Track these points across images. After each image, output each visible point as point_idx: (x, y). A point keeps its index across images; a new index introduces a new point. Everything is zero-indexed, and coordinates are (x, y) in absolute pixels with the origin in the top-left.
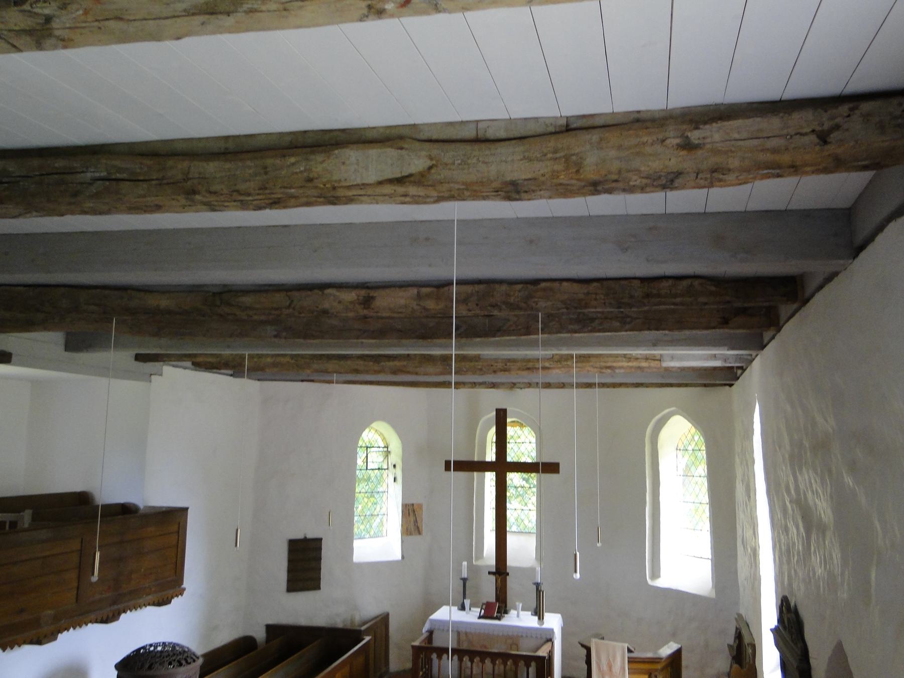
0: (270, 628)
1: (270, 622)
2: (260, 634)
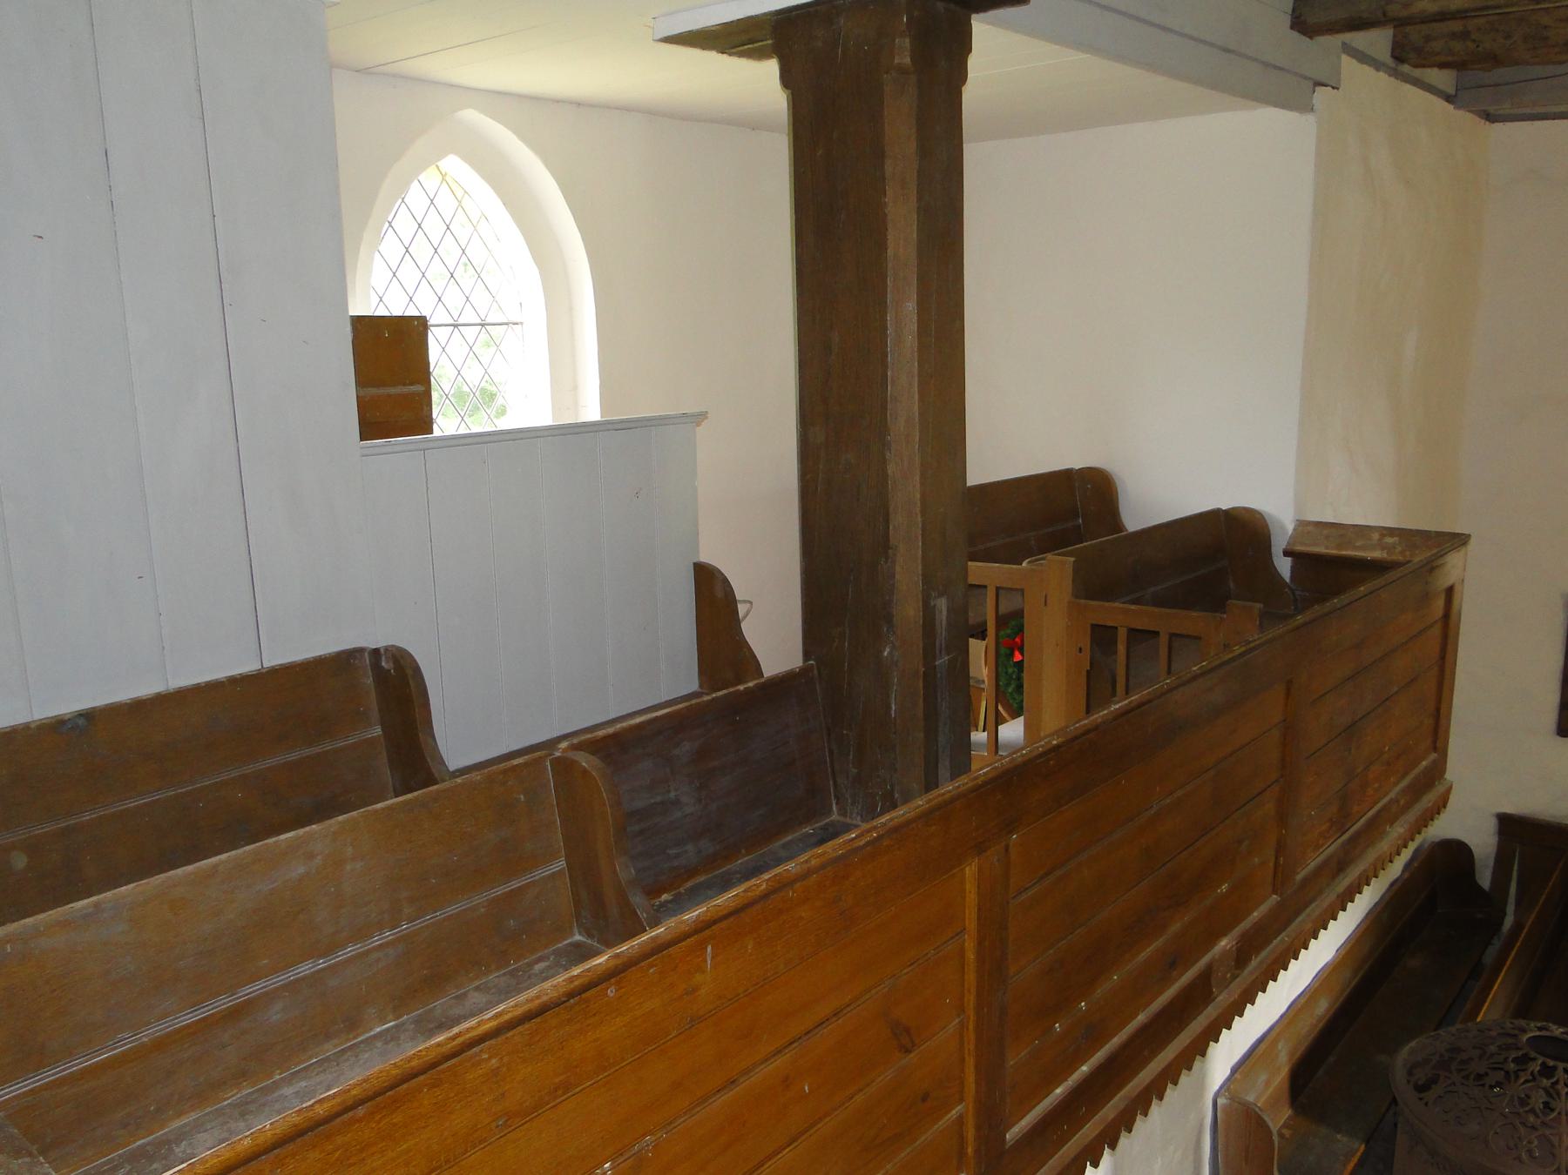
0: (1510, 826)
1: (1509, 809)
2: (1482, 840)
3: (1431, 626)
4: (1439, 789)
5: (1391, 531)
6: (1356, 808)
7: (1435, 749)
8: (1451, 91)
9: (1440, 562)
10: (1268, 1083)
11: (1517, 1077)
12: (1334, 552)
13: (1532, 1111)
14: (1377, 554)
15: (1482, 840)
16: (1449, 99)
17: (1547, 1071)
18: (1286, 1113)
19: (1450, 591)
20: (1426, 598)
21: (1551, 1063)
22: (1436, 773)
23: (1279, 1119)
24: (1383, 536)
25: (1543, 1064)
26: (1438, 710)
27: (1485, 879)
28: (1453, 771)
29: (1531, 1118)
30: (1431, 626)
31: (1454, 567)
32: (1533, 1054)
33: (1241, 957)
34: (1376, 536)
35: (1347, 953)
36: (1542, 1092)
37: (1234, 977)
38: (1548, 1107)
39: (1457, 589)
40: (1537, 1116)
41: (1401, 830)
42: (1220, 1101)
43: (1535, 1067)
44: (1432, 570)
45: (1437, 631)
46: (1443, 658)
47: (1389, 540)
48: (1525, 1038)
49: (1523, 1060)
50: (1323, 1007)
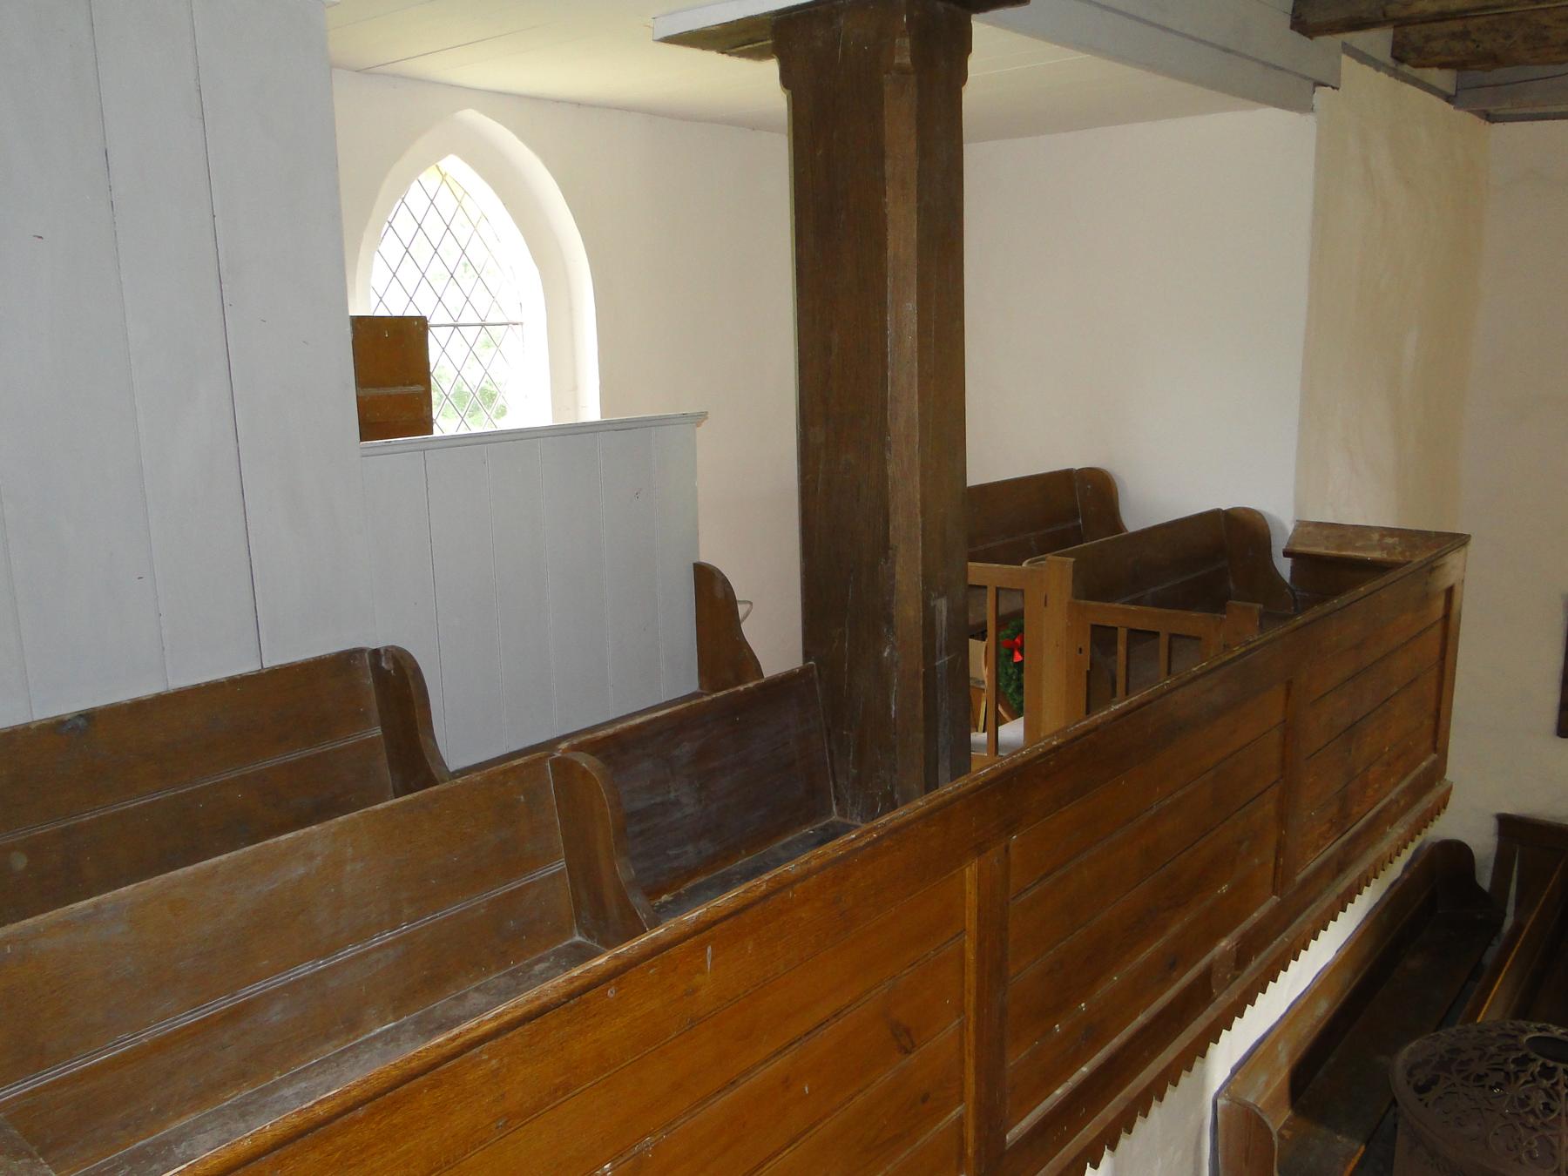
0: (1510, 827)
1: (1509, 809)
2: (1482, 841)
3: (1431, 626)
4: (1439, 790)
5: (1391, 532)
6: (1356, 809)
7: (1435, 750)
8: (1452, 91)
9: (1440, 562)
10: (1268, 1084)
11: (1517, 1078)
12: (1334, 552)
13: (1533, 1112)
14: (1377, 555)
15: (1482, 841)
16: (1449, 99)
17: (1547, 1072)
18: (1286, 1113)
19: (1450, 591)
20: (1426, 598)
21: (1551, 1064)
22: (1436, 773)
23: (1279, 1120)
24: (1382, 536)
25: (1543, 1065)
26: (1438, 710)
27: (1485, 880)
28: (1453, 772)
29: (1532, 1120)
30: (1431, 626)
31: (1454, 567)
32: (1533, 1055)
33: (1241, 958)
34: (1376, 536)
35: (1348, 954)
36: (1542, 1093)
37: (1234, 978)
38: (1548, 1108)
39: (1457, 589)
40: (1537, 1117)
41: (1401, 831)
42: (1220, 1102)
43: (1535, 1068)
44: (1432, 570)
45: (1437, 631)
46: (1443, 658)
47: (1390, 541)
48: (1525, 1039)
49: (1524, 1061)
50: (1323, 1008)
